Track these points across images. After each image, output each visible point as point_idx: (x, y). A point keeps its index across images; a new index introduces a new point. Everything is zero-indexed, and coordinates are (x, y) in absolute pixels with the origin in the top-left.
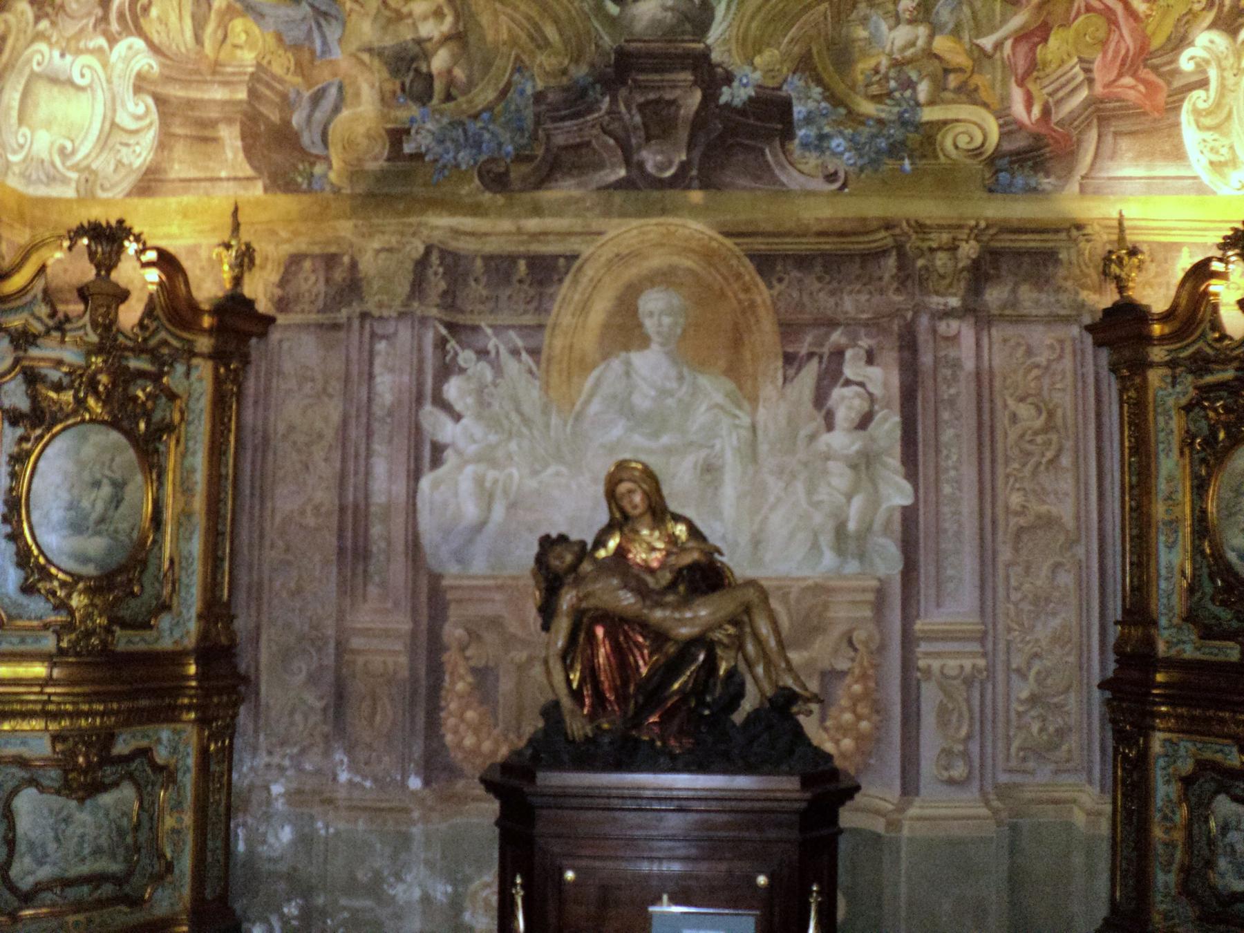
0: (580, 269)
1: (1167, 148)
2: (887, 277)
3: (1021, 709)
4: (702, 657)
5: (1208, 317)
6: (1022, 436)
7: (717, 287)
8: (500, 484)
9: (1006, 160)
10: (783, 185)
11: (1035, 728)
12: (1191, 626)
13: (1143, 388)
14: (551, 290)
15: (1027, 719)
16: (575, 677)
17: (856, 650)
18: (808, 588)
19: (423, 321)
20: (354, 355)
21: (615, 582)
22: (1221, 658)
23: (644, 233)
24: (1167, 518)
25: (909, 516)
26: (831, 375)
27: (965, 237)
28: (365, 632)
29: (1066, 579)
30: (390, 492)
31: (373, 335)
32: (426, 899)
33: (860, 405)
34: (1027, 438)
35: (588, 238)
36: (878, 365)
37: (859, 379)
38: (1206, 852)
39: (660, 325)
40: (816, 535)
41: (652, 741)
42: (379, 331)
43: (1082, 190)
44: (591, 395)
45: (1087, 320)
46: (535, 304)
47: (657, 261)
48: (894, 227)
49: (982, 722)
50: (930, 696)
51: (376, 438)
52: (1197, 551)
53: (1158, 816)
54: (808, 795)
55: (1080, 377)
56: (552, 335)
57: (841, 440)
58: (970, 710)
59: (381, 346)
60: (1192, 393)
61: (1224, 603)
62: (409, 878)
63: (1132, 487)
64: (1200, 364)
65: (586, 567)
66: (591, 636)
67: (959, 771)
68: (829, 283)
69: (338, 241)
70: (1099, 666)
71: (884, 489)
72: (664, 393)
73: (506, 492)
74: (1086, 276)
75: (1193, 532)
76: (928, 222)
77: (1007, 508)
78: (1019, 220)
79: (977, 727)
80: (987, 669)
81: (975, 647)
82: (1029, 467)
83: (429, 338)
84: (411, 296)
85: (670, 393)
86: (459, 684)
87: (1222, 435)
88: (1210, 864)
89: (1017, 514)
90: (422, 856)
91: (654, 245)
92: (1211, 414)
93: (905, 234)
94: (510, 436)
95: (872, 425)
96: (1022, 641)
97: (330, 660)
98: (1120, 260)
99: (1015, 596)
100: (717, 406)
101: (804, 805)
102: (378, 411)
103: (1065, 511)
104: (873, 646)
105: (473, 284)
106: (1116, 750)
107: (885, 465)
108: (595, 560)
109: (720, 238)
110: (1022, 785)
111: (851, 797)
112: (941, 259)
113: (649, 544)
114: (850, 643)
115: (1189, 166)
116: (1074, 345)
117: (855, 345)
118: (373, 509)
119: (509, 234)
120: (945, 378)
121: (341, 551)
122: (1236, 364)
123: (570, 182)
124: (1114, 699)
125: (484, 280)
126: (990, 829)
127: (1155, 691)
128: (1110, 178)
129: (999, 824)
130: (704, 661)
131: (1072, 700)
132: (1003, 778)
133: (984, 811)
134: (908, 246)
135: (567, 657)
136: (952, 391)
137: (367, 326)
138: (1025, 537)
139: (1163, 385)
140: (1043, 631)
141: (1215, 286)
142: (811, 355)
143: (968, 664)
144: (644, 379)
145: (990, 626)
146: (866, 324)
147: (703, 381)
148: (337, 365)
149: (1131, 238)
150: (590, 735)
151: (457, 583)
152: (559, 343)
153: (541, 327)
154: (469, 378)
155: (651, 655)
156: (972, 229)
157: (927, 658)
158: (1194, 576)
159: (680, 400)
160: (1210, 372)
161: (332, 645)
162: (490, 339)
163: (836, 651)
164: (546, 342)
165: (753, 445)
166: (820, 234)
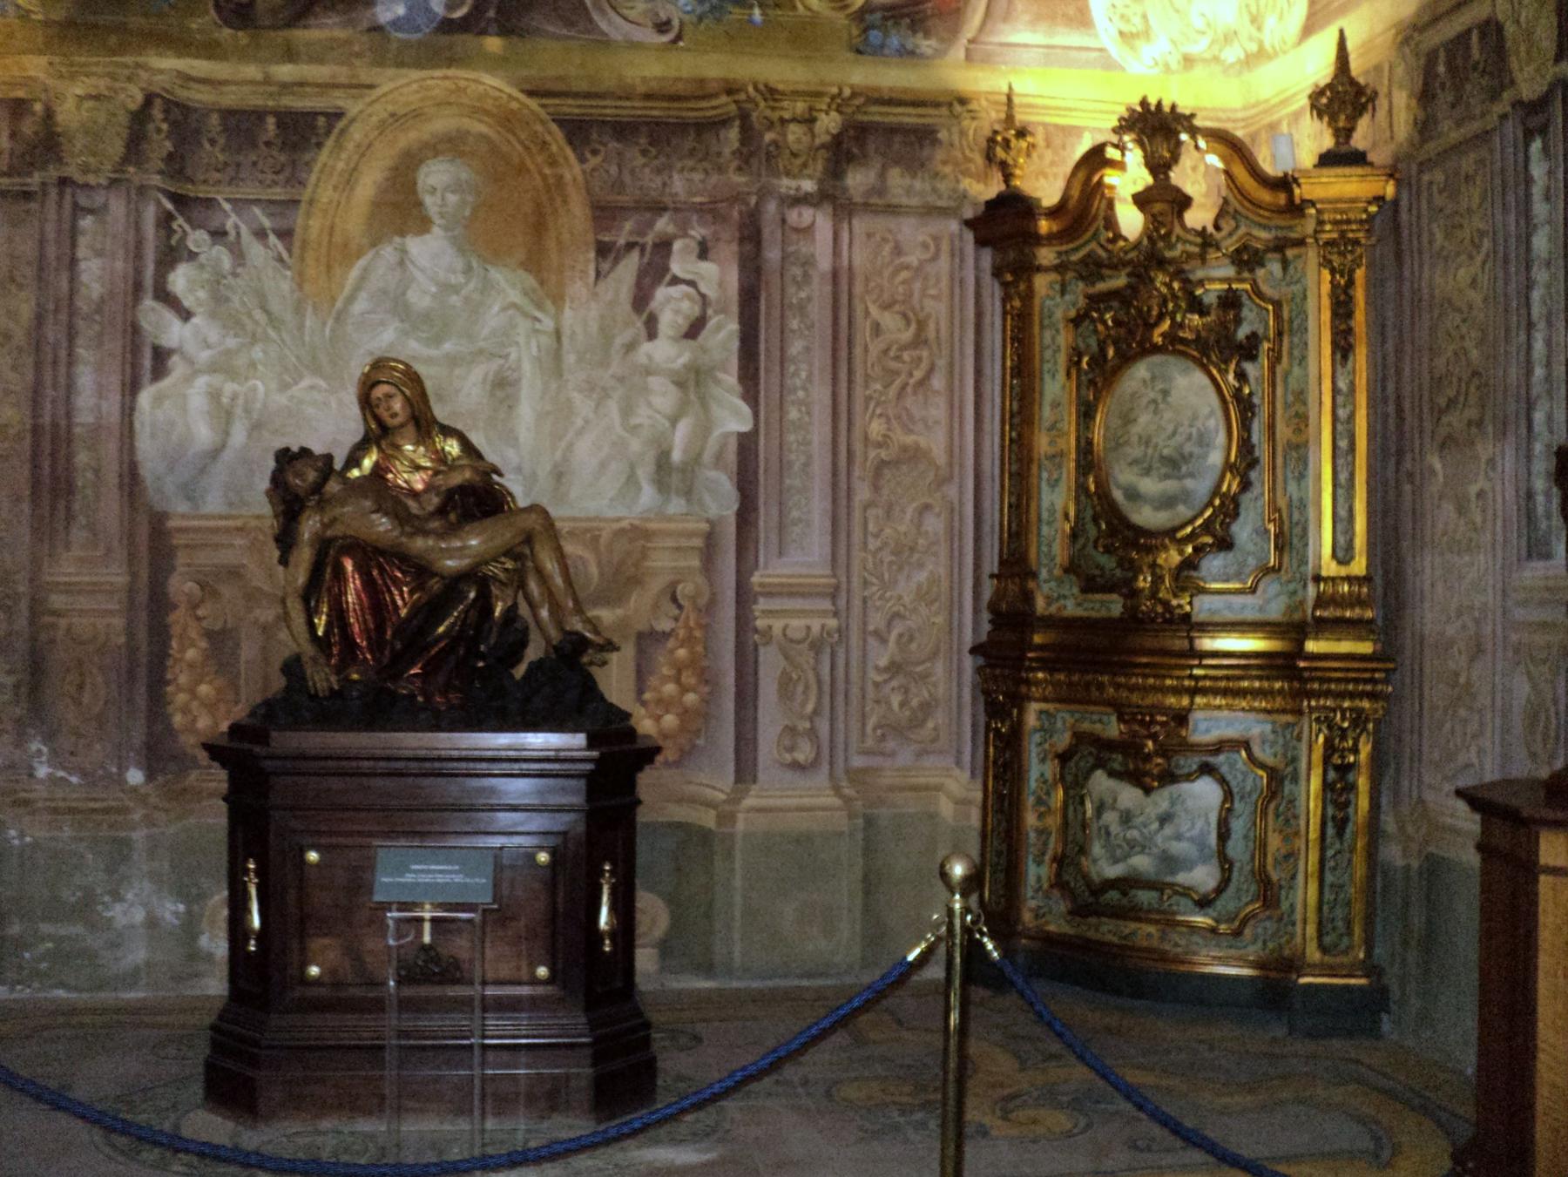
0: (343, 132)
1: (1071, 11)
2: (727, 151)
3: (879, 679)
4: (472, 595)
5: (1102, 214)
6: (886, 352)
7: (516, 160)
8: (241, 401)
9: (878, 15)
10: (604, 34)
11: (896, 700)
12: (1074, 578)
13: (1028, 296)
14: (307, 157)
15: (887, 689)
16: (321, 623)
17: (680, 607)
18: (622, 531)
19: (142, 190)
20: (50, 229)
21: (368, 504)
22: (1103, 613)
23: (428, 89)
24: (1051, 451)
25: (747, 445)
26: (655, 271)
27: (824, 107)
28: (69, 589)
29: (934, 524)
30: (99, 407)
31: (75, 205)
32: (152, 923)
33: (690, 309)
34: (892, 354)
35: (354, 91)
36: (713, 261)
37: (688, 277)
38: (1080, 834)
39: (444, 205)
40: (632, 467)
41: (412, 697)
42: (83, 201)
43: (969, 57)
44: (357, 288)
45: (969, 213)
46: (287, 173)
47: (443, 123)
48: (738, 91)
49: (832, 696)
50: (770, 664)
51: (80, 341)
52: (1081, 488)
53: (1031, 800)
54: (595, 754)
55: (957, 281)
56: (308, 215)
57: (665, 351)
58: (819, 682)
59: (86, 222)
60: (1082, 302)
61: (1108, 550)
62: (130, 896)
63: (1012, 416)
64: (1092, 269)
65: (333, 486)
66: (339, 573)
67: (804, 753)
68: (656, 157)
69: (28, 81)
70: (971, 627)
71: (717, 411)
72: (447, 288)
73: (247, 411)
74: (970, 160)
75: (1078, 466)
76: (781, 87)
77: (866, 438)
78: (891, 89)
79: (826, 700)
80: (839, 630)
81: (826, 605)
82: (892, 392)
83: (150, 214)
84: (125, 160)
85: (455, 289)
86: (189, 652)
87: (1111, 352)
88: (1083, 850)
89: (879, 445)
90: (145, 868)
91: (439, 105)
92: (1100, 327)
93: (750, 99)
94: (254, 339)
95: (704, 333)
96: (880, 598)
97: (22, 622)
98: (1007, 142)
99: (873, 544)
100: (514, 305)
101: (589, 767)
102: (82, 305)
103: (936, 443)
104: (703, 601)
105: (207, 146)
106: (988, 726)
107: (718, 382)
108: (346, 481)
109: (522, 97)
110: (877, 770)
111: (651, 761)
112: (795, 133)
113: (412, 461)
114: (674, 599)
115: (1096, 36)
116: (952, 242)
117: (686, 235)
118: (78, 430)
119: (252, 82)
120: (794, 278)
121: (36, 483)
122: (1128, 269)
123: (332, 19)
124: (989, 665)
125: (222, 141)
126: (841, 822)
127: (1030, 655)
128: (1002, 45)
129: (851, 816)
130: (475, 600)
131: (939, 668)
132: (858, 762)
133: (836, 802)
134: (755, 115)
135: (309, 595)
136: (803, 295)
137: (68, 198)
138: (887, 473)
139: (1051, 293)
140: (906, 588)
141: (1111, 177)
142: (630, 246)
143: (816, 625)
144: (422, 270)
145: (844, 579)
146: (700, 209)
147: (496, 275)
148: (28, 248)
149: (1021, 117)
150: (336, 687)
151: (185, 523)
152: (315, 224)
153: (296, 202)
154: (202, 267)
155: (411, 593)
156: (833, 98)
157: (767, 616)
158: (1077, 517)
159: (467, 300)
160: (1102, 278)
161: (24, 605)
162: (227, 216)
163: (656, 606)
164: (300, 221)
165: (557, 355)
166: (648, 96)
